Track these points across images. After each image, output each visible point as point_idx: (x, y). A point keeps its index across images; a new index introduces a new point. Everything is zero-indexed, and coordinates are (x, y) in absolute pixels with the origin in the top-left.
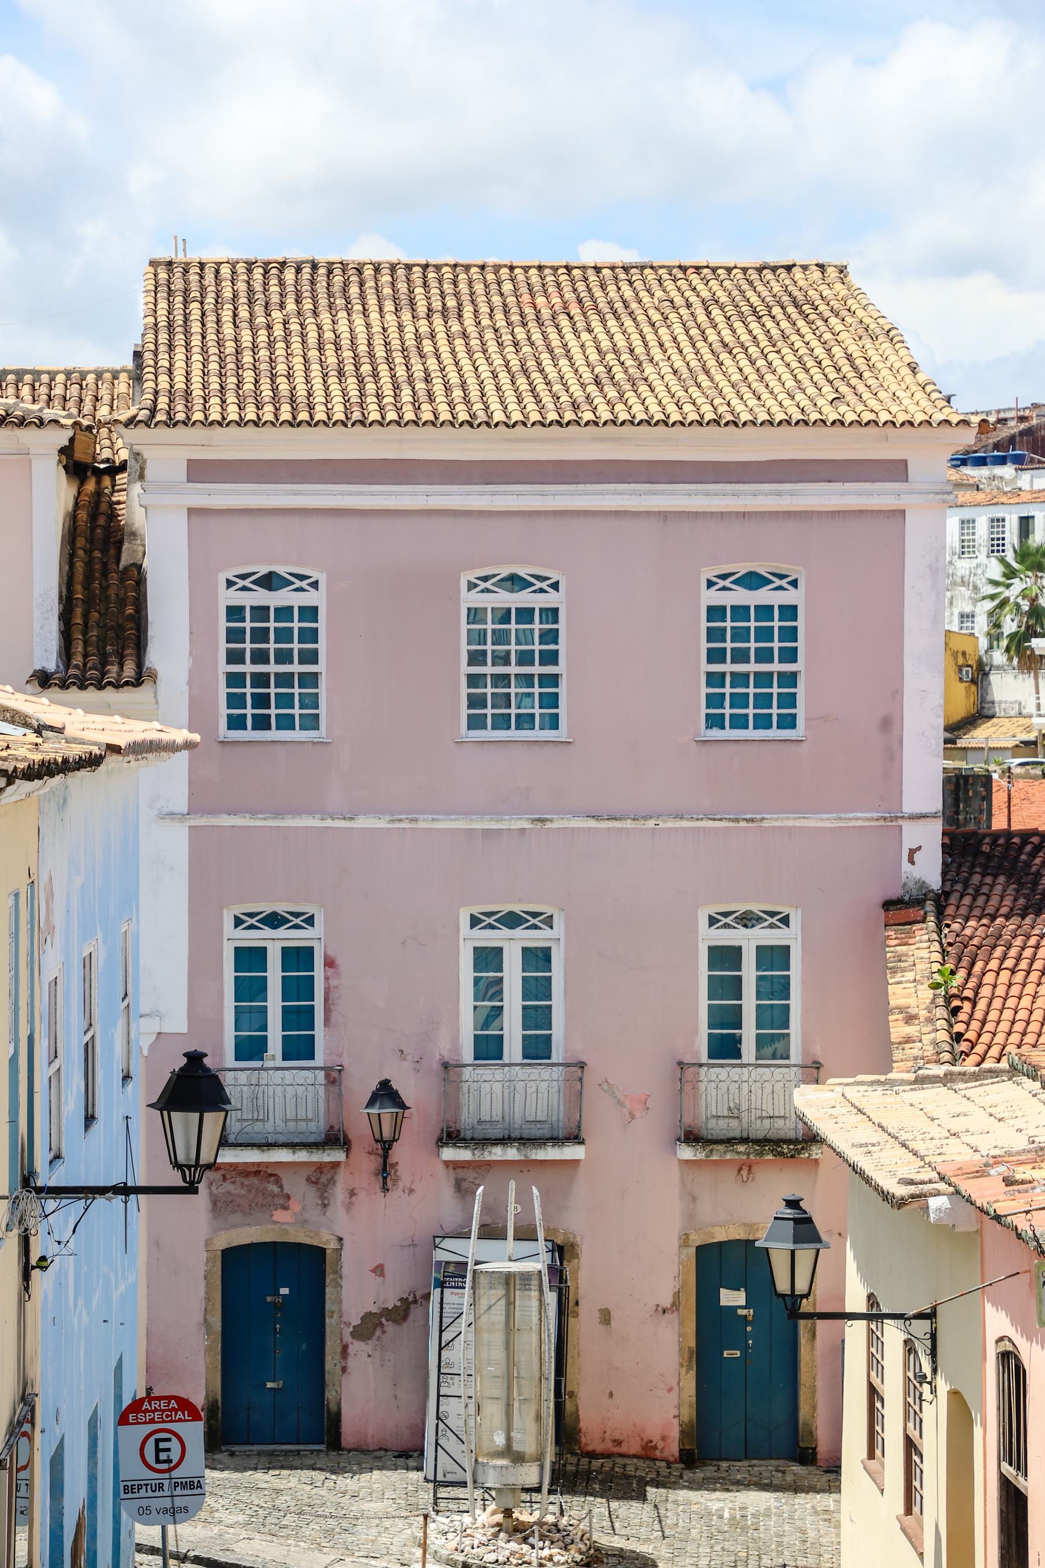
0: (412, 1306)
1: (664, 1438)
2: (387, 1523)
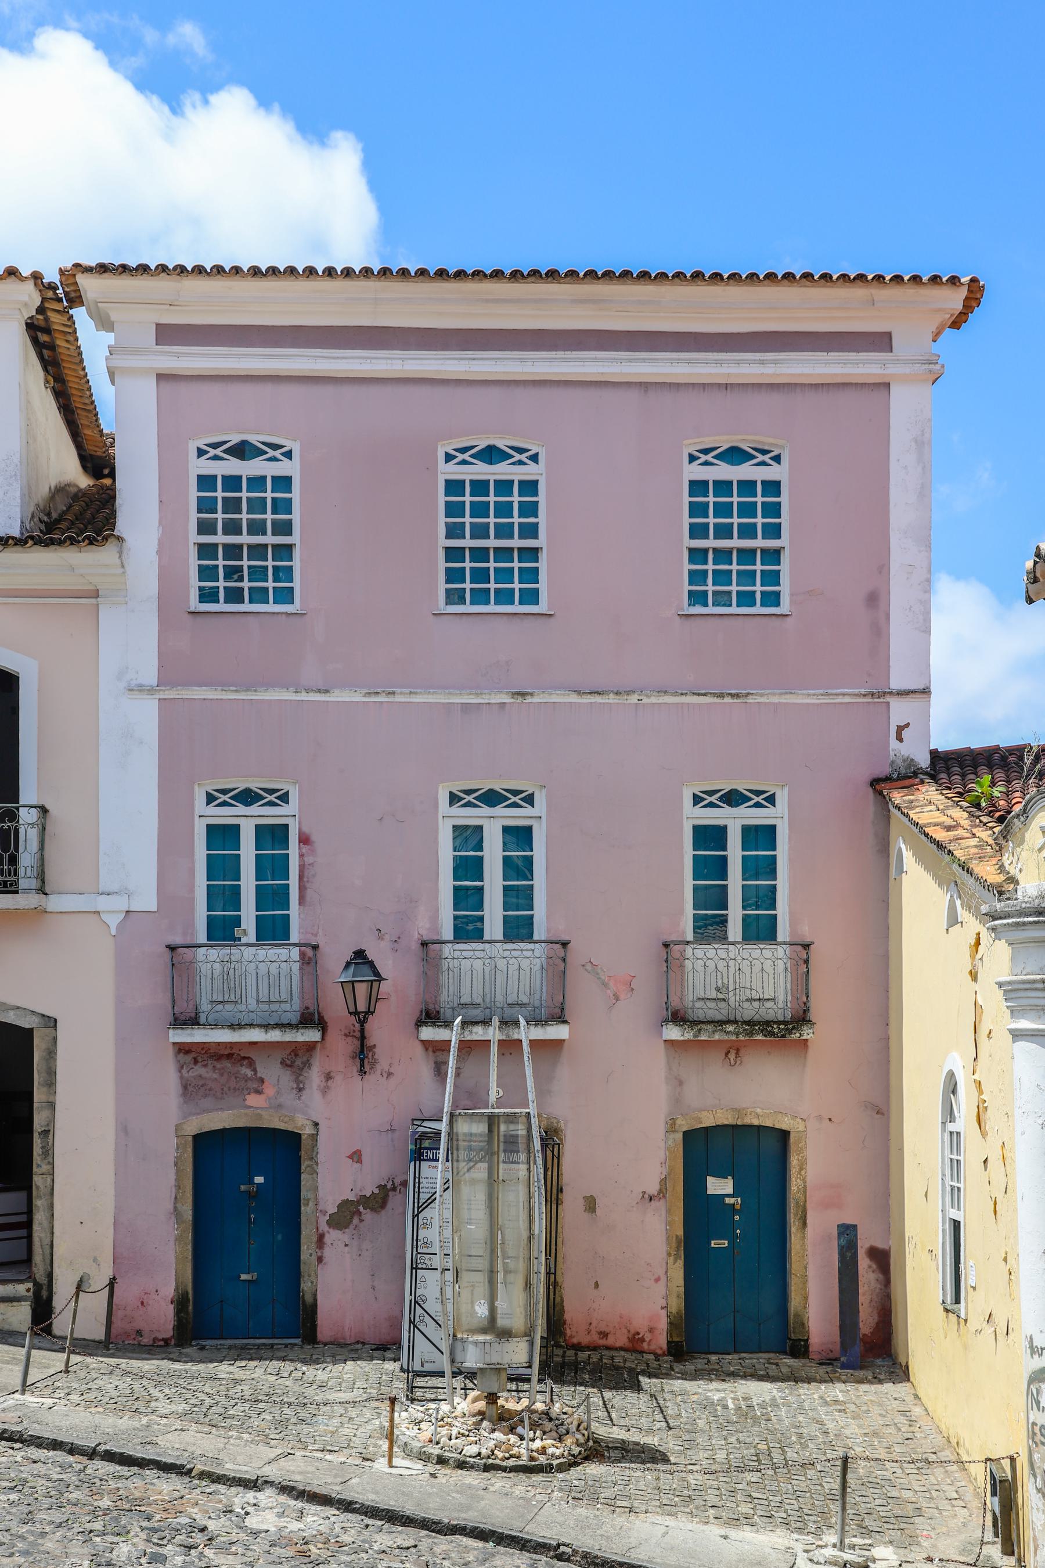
0: (391, 1193)
1: (651, 1330)
2: (353, 1413)
